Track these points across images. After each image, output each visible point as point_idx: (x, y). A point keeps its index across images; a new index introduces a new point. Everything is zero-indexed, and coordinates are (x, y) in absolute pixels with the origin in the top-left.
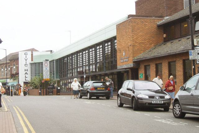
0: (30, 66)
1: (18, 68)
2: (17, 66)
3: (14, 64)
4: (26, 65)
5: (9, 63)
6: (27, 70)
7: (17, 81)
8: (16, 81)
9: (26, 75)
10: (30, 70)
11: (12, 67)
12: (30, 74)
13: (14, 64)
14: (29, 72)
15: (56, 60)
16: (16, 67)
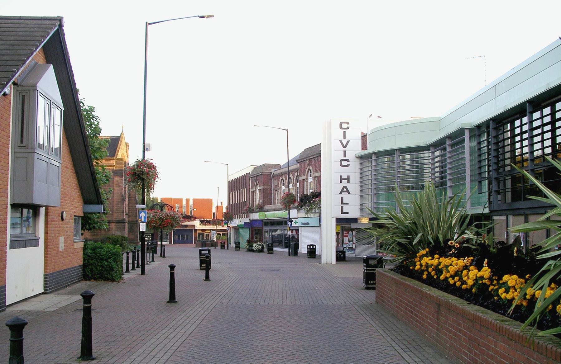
0: (358, 167)
1: (318, 180)
2: (317, 174)
3: (309, 169)
4: (344, 163)
5: (297, 170)
6: (348, 180)
7: (317, 215)
8: (312, 215)
9: (344, 195)
10: (358, 180)
11: (305, 177)
12: (358, 193)
13: (309, 169)
14: (354, 186)
15: (471, 130)
16: (315, 177)
